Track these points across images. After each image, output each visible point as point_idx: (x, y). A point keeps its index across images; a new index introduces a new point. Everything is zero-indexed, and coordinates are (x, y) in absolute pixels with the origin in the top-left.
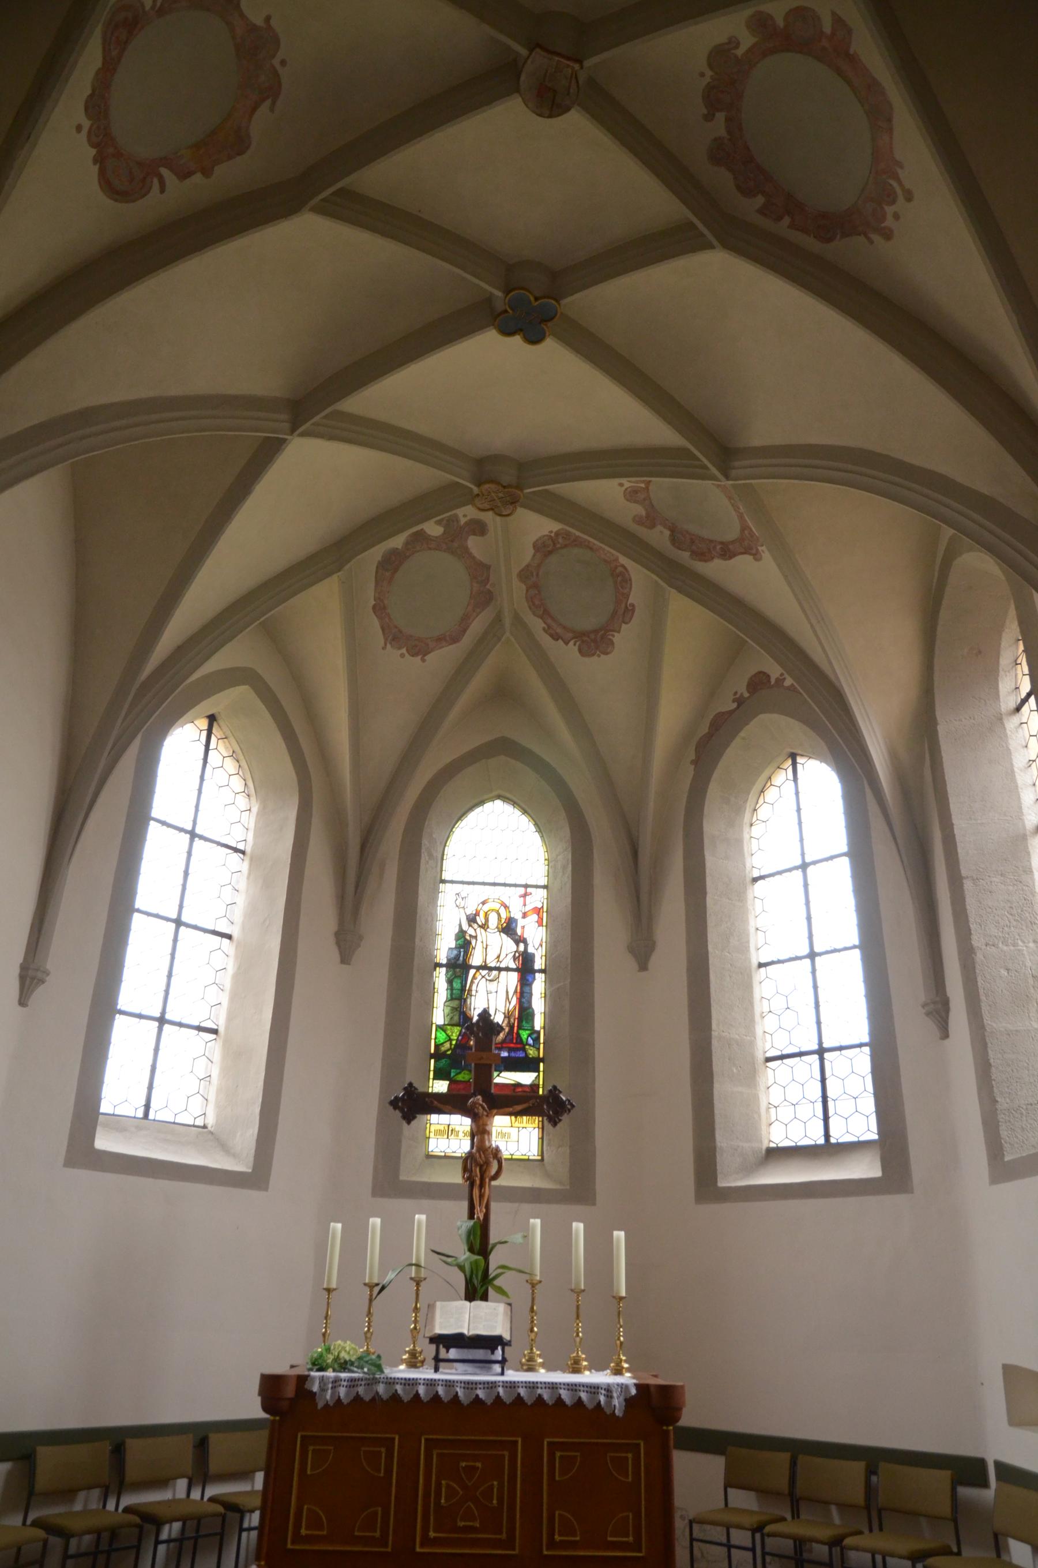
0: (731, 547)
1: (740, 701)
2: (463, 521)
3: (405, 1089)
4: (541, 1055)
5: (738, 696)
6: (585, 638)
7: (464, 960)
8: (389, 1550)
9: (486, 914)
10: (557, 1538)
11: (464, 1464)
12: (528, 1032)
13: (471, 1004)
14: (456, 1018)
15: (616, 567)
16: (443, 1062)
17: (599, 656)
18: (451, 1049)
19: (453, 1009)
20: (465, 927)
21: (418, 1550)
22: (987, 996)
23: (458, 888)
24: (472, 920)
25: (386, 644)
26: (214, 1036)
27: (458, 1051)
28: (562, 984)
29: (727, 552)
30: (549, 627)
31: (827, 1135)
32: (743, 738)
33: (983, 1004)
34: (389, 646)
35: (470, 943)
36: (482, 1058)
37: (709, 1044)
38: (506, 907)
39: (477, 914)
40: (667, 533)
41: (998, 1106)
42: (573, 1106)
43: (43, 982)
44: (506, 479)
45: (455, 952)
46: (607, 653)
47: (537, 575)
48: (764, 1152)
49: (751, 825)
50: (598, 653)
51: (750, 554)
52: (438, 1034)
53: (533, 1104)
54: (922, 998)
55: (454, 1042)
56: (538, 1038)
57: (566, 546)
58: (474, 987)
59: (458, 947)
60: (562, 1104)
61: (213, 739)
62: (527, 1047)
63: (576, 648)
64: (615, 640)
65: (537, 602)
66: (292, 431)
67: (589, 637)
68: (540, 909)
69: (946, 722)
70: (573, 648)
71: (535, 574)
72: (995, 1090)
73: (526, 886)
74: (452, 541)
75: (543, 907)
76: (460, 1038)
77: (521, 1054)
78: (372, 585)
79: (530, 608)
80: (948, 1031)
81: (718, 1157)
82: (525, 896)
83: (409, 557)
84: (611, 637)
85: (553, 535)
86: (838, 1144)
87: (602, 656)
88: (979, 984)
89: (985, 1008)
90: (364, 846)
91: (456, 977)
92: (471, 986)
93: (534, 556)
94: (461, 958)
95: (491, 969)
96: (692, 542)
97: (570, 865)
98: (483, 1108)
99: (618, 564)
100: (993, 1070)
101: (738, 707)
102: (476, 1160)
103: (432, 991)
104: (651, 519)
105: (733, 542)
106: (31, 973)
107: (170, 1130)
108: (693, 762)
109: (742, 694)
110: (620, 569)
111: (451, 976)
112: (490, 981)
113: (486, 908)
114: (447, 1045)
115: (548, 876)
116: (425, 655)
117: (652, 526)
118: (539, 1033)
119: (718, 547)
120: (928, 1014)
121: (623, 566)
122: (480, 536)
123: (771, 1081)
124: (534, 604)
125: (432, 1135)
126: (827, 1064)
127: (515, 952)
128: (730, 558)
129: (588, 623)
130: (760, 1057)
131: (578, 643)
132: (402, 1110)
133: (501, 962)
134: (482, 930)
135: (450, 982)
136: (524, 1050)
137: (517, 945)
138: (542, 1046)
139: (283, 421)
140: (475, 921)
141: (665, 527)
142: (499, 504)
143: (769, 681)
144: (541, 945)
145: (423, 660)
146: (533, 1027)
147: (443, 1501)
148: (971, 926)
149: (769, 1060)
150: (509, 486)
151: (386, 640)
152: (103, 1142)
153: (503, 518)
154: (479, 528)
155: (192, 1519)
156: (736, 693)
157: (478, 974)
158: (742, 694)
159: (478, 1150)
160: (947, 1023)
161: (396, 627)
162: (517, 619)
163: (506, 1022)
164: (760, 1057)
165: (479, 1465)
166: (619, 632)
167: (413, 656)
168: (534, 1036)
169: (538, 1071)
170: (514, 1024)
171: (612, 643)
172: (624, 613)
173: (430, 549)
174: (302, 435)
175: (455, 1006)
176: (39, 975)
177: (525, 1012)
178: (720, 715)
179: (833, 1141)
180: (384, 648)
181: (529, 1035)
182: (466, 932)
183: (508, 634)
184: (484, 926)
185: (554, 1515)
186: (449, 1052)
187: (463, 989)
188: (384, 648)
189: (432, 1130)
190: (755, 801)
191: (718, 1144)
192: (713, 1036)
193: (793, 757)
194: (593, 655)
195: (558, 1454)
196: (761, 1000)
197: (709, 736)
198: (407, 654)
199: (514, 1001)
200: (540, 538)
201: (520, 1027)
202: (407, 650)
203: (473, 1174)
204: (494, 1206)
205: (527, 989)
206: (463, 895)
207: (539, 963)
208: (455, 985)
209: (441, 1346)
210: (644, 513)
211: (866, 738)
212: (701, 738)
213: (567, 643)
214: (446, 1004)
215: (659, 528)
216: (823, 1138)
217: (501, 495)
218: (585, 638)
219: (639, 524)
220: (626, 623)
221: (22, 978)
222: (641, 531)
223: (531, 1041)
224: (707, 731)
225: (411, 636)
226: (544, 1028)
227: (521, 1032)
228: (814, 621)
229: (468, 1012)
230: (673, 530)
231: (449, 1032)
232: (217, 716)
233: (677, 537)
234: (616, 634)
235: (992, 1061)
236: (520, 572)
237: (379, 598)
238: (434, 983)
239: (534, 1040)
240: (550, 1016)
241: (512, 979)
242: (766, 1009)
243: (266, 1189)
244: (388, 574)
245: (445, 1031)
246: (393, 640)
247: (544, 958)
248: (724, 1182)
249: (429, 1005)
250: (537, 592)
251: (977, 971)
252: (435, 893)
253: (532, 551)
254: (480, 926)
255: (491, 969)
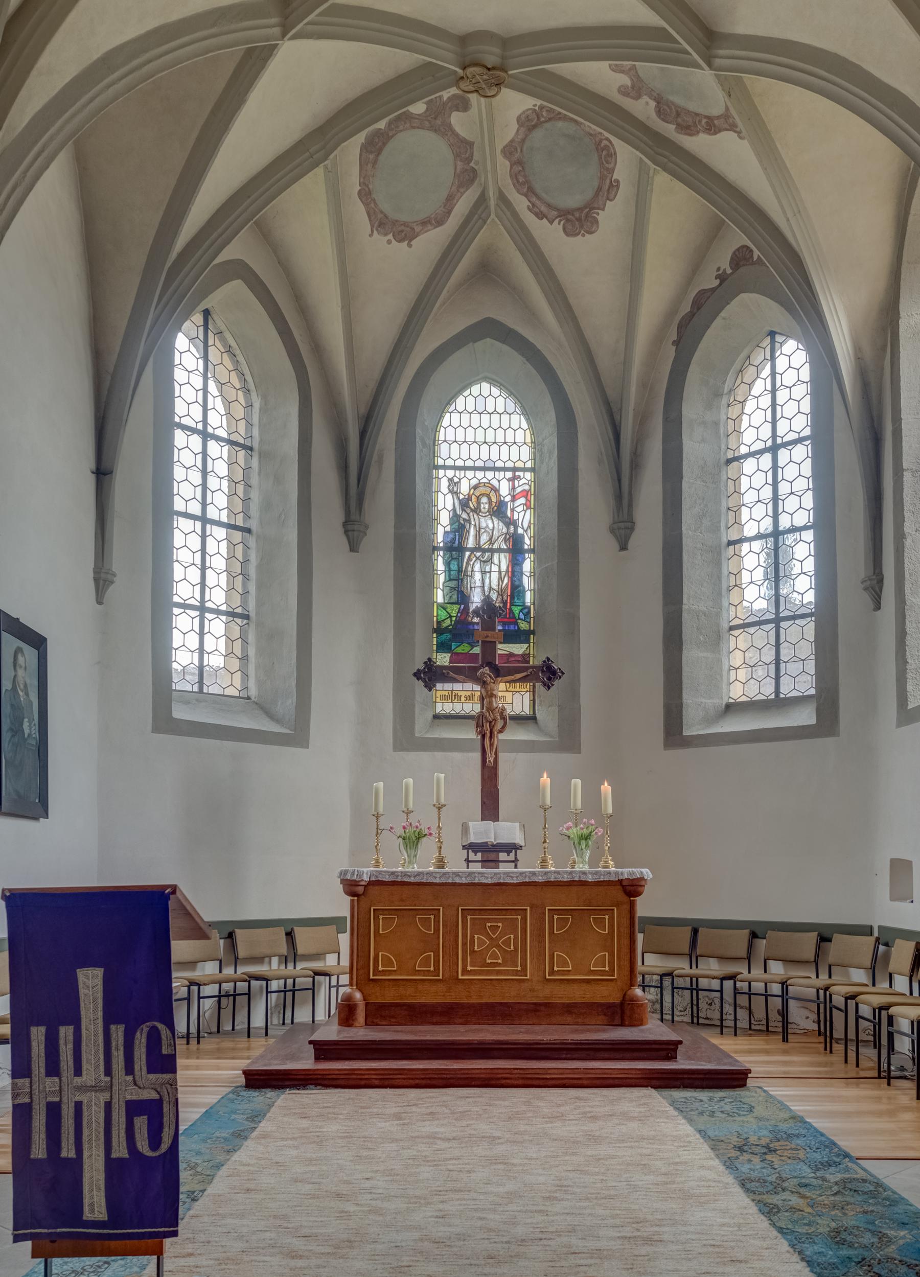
0: (716, 122)
1: (722, 278)
2: (445, 98)
3: (425, 663)
4: (532, 628)
5: (720, 272)
6: (570, 217)
7: (460, 543)
8: (441, 978)
9: (478, 498)
10: (556, 969)
11: (489, 924)
12: (520, 608)
13: (467, 583)
14: (455, 597)
15: (601, 141)
16: (446, 637)
17: (583, 235)
18: (451, 625)
19: (452, 589)
20: (459, 512)
21: (460, 977)
22: (911, 575)
23: (450, 473)
24: (464, 504)
25: (372, 231)
26: (245, 621)
27: (458, 626)
28: (550, 564)
29: (712, 127)
30: (533, 205)
31: (777, 691)
32: (724, 319)
33: (906, 583)
34: (375, 232)
35: (463, 526)
36: (487, 636)
37: (681, 616)
38: (496, 491)
39: (469, 498)
40: (653, 104)
41: (908, 667)
42: (563, 673)
43: (112, 582)
44: (491, 60)
45: (451, 536)
46: (591, 233)
47: (522, 151)
48: (723, 707)
49: (729, 405)
50: (582, 232)
51: (735, 132)
52: (440, 612)
53: (531, 673)
54: (862, 575)
55: (454, 619)
56: (529, 612)
57: (550, 119)
58: (470, 569)
59: (454, 531)
60: (554, 673)
61: (210, 334)
62: (519, 621)
63: (561, 226)
64: (599, 218)
65: (521, 179)
66: (284, 35)
67: (573, 215)
68: (528, 492)
69: (908, 316)
70: (558, 227)
71: (519, 150)
72: (908, 653)
73: (514, 469)
74: (435, 118)
75: (530, 489)
76: (459, 614)
77: (514, 628)
78: (356, 170)
79: (514, 185)
80: (880, 603)
81: (684, 712)
82: (512, 480)
83: (392, 136)
84: (595, 215)
85: (537, 108)
86: (786, 699)
87: (586, 235)
88: (906, 565)
89: (908, 586)
90: (363, 434)
91: (453, 559)
92: (467, 567)
93: (518, 131)
94: (457, 542)
95: (484, 551)
96: (678, 114)
97: (556, 450)
98: (490, 677)
99: (603, 138)
100: (908, 637)
101: (720, 284)
102: (486, 718)
103: (431, 572)
104: (637, 90)
105: (718, 117)
106: (103, 575)
107: (220, 700)
108: (674, 343)
109: (725, 270)
110: (605, 142)
111: (448, 558)
112: (484, 562)
113: (477, 493)
114: (448, 622)
115: (535, 459)
116: (411, 240)
117: (638, 97)
118: (529, 608)
119: (704, 121)
120: (866, 589)
121: (607, 139)
122: (463, 112)
123: (732, 646)
124: (518, 181)
125: (438, 700)
126: (782, 631)
127: (506, 534)
128: (715, 133)
129: (573, 201)
130: (725, 626)
131: (562, 223)
132: (424, 681)
133: (493, 544)
134: (475, 516)
135: (447, 564)
136: (517, 624)
137: (508, 528)
138: (532, 619)
139: (274, 26)
140: (468, 506)
141: (650, 98)
142: (484, 86)
143: (752, 257)
144: (529, 527)
145: (410, 246)
146: (524, 603)
147: (476, 948)
148: (905, 513)
149: (731, 628)
150: (494, 68)
151: (372, 226)
152: (180, 713)
153: (487, 99)
154: (462, 105)
155: (227, 1033)
156: (719, 269)
157: (473, 555)
158: (725, 270)
159: (488, 710)
160: (880, 598)
161: (382, 212)
162: (502, 198)
163: (500, 599)
164: (725, 626)
165: (500, 924)
166: (603, 209)
167: (399, 242)
168: (526, 610)
169: (529, 643)
170: (507, 601)
171: (596, 221)
172: (608, 190)
173: (413, 128)
174: (293, 38)
175: (453, 586)
176: (109, 577)
177: (516, 590)
178: (702, 293)
179: (782, 696)
180: (371, 235)
181: (521, 611)
182: (460, 516)
183: (493, 216)
184: (477, 510)
185: (553, 954)
186: (451, 627)
187: (459, 570)
188: (371, 235)
189: (438, 695)
190: (734, 381)
191: (684, 701)
192: (683, 609)
193: (772, 334)
194: (578, 234)
195: (556, 917)
196: (728, 576)
197: (691, 315)
198: (394, 241)
199: (506, 581)
200: (524, 112)
201: (512, 604)
202: (393, 236)
203: (485, 728)
204: (500, 755)
205: (517, 569)
206: (456, 480)
207: (528, 542)
208: (452, 566)
209: (470, 851)
210: (629, 83)
211: (831, 331)
212: (683, 317)
213: (551, 222)
214: (445, 584)
215: (645, 98)
216: (774, 694)
217: (485, 77)
218: (570, 217)
219: (624, 95)
220: (611, 200)
221: (96, 580)
222: (627, 103)
223: (522, 616)
224: (688, 309)
225: (397, 221)
226: (534, 604)
227: (513, 608)
228: (790, 215)
229: (465, 591)
230: (659, 100)
231: (448, 610)
232: (211, 310)
233: (664, 109)
234: (600, 211)
235: (907, 630)
236: (504, 148)
237: (365, 184)
238: (433, 566)
239: (525, 615)
240: (539, 593)
241: (503, 561)
242: (732, 583)
243: (307, 747)
244: (372, 157)
245: (445, 609)
246: (379, 226)
247: (532, 539)
248: (691, 730)
249: (430, 586)
250: (521, 169)
251: (906, 554)
252: (429, 479)
253: (515, 126)
254: (472, 510)
255: (484, 551)
